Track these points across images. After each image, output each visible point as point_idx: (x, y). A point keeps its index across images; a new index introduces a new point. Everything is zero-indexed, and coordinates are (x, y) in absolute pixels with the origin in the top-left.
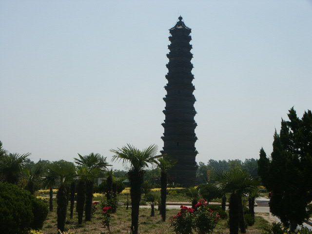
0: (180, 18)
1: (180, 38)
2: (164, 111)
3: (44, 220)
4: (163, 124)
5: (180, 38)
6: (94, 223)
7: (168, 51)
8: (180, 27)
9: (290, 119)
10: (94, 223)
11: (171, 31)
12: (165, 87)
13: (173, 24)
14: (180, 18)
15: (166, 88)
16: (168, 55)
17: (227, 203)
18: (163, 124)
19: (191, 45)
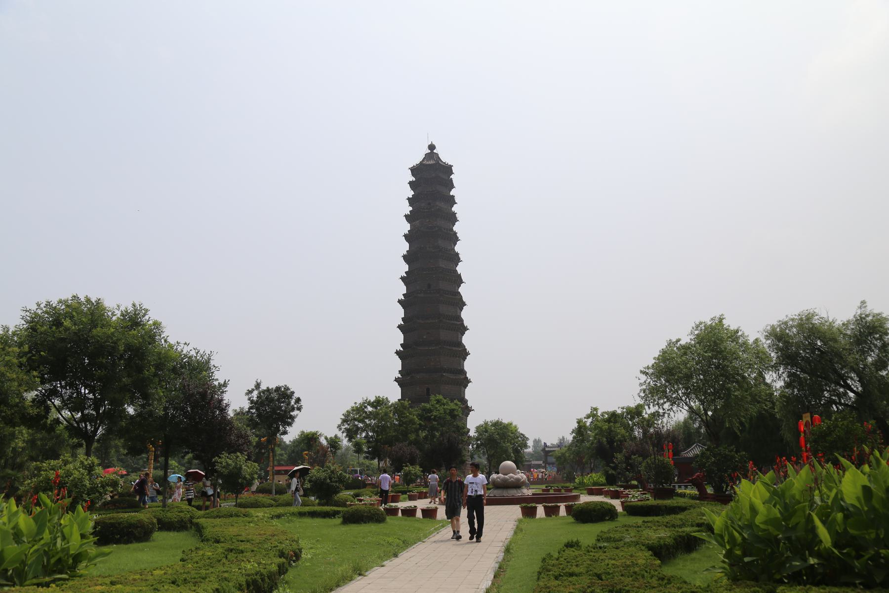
0: (432, 147)
1: (432, 185)
2: (399, 327)
3: (172, 354)
4: (397, 353)
5: (432, 185)
6: (599, 577)
7: (408, 209)
8: (431, 162)
9: (483, 429)
10: (599, 577)
11: (414, 170)
12: (405, 236)
13: (417, 158)
14: (432, 147)
15: (406, 237)
16: (406, 237)
17: (851, 483)
18: (397, 353)
19: (453, 196)
